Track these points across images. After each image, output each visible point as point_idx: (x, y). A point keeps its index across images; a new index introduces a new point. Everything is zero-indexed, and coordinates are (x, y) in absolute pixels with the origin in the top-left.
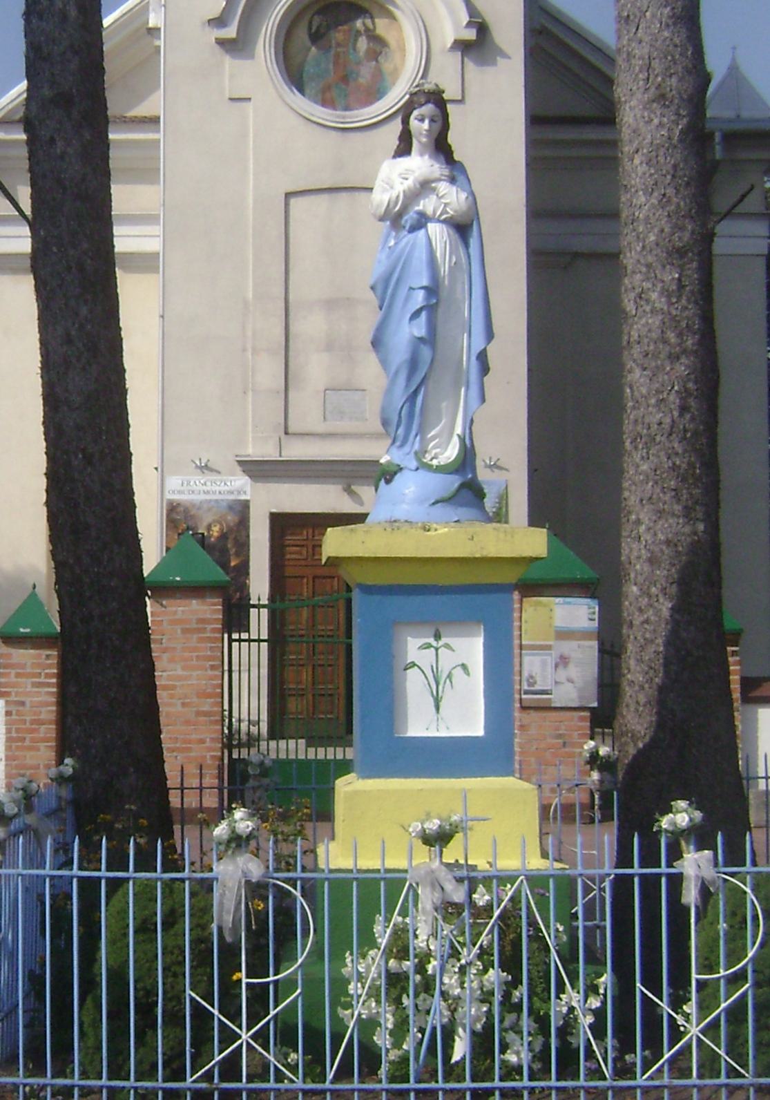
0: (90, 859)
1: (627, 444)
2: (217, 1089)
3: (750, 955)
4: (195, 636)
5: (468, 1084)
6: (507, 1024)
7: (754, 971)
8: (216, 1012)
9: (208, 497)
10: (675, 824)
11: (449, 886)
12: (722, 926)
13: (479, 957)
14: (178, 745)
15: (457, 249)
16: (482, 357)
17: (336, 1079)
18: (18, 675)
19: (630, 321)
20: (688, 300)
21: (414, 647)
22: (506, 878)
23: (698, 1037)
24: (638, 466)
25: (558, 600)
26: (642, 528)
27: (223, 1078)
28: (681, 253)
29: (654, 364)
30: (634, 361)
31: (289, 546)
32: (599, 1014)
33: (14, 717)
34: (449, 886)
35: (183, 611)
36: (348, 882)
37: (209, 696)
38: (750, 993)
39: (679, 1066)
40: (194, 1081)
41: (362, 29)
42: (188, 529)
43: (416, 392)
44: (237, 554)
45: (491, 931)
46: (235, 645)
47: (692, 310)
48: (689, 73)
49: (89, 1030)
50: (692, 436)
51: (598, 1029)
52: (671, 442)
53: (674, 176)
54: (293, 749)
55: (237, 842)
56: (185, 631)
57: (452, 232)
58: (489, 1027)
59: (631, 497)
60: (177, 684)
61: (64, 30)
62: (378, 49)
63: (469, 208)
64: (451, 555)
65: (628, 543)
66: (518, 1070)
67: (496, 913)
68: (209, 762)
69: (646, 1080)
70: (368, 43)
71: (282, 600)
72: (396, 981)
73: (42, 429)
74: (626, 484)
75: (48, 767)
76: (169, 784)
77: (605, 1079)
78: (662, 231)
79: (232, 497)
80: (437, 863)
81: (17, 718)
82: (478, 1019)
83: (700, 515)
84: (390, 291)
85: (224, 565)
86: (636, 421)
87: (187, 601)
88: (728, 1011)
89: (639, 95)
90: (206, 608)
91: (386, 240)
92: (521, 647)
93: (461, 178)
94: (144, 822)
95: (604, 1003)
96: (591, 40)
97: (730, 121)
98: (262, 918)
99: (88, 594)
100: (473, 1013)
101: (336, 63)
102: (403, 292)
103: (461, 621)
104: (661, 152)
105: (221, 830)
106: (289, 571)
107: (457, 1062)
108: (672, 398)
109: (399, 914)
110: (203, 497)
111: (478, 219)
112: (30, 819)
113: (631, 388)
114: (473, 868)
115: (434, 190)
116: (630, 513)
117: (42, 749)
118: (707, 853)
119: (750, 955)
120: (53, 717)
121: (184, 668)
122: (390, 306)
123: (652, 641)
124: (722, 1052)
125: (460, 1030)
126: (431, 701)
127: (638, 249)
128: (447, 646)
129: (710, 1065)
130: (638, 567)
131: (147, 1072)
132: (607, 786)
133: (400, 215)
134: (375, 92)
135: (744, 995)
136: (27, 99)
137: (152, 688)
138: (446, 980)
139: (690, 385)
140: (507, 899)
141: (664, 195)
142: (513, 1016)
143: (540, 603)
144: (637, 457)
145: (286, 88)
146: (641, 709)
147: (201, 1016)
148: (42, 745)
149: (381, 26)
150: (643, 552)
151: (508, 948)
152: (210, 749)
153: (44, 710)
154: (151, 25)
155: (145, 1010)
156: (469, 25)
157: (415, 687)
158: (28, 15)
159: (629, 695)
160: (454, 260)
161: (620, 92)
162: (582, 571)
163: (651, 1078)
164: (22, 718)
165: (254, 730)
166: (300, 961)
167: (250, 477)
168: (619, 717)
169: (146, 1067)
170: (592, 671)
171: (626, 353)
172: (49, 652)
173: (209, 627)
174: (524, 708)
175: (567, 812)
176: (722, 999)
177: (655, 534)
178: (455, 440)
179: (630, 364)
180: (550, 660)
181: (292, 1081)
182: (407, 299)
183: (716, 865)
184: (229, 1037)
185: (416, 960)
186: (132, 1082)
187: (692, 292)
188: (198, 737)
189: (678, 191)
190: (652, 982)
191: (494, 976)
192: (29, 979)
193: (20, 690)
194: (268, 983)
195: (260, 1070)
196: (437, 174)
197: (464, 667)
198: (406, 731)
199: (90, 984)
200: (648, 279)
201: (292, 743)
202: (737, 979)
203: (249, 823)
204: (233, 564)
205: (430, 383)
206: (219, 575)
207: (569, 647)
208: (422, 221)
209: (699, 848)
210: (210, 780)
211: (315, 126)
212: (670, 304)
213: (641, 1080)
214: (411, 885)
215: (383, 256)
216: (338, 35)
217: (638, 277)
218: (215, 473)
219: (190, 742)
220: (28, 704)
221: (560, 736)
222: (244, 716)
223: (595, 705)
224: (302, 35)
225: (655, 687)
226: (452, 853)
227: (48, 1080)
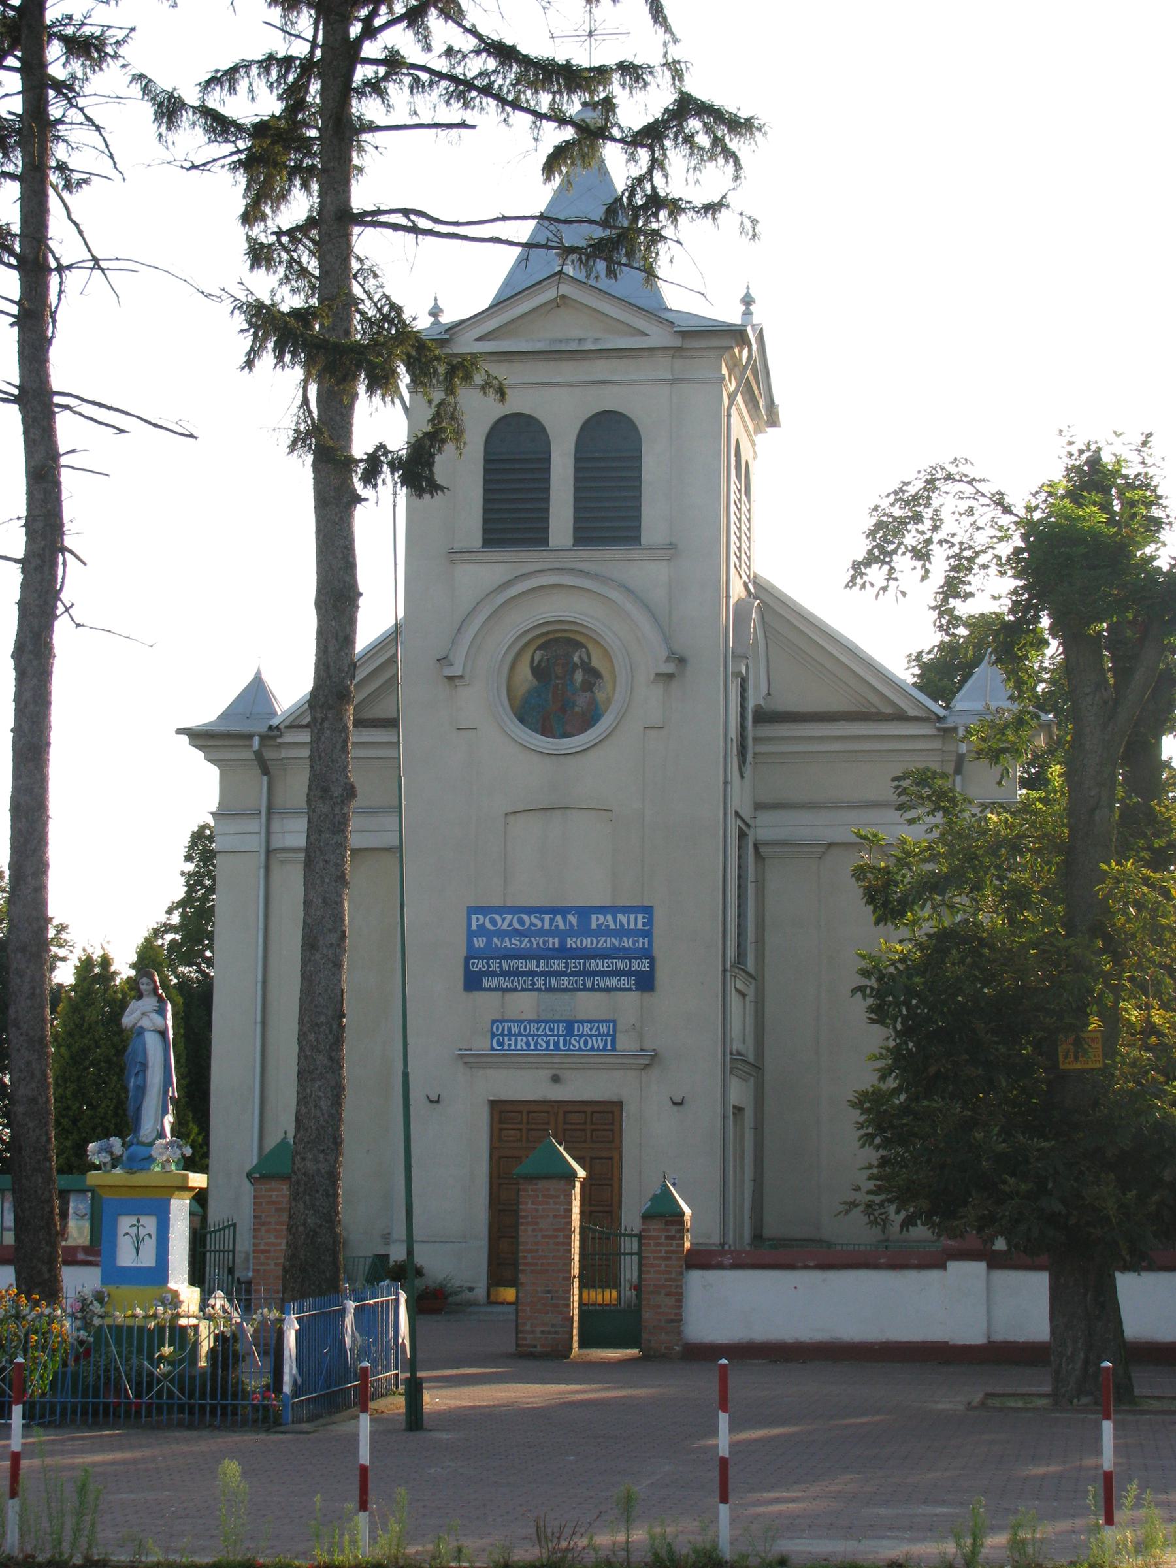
56: (277, 1210)
62: (592, 680)
70: (584, 675)
96: (843, 641)
126: (135, 1251)
213: (146, 1400)
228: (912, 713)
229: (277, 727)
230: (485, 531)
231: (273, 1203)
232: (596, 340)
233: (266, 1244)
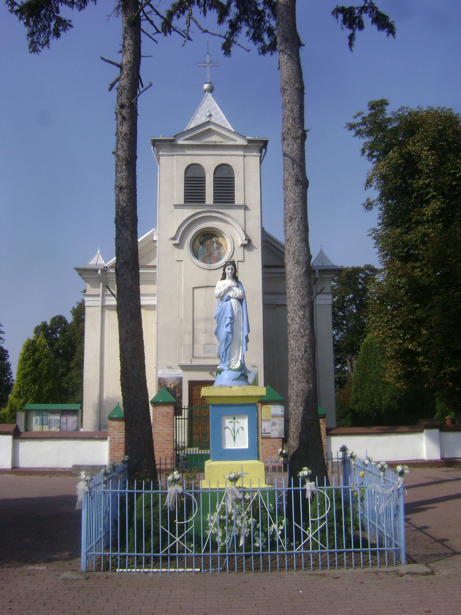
0: (131, 487)
1: (290, 362)
2: (169, 555)
3: (326, 513)
5: (244, 553)
6: (255, 534)
7: (327, 518)
8: (169, 532)
10: (304, 474)
11: (237, 494)
12: (318, 504)
13: (247, 514)
15: (239, 306)
16: (247, 337)
17: (205, 551)
18: (113, 429)
19: (290, 326)
20: (307, 320)
21: (228, 422)
22: (254, 491)
23: (312, 538)
24: (293, 368)
25: (272, 406)
26: (294, 386)
27: (171, 552)
28: (304, 306)
29: (297, 338)
30: (291, 337)
32: (283, 531)
34: (237, 494)
36: (208, 493)
37: (170, 435)
38: (327, 524)
39: (306, 546)
40: (162, 553)
42: (164, 386)
43: (227, 348)
44: (179, 393)
45: (250, 507)
46: (178, 420)
47: (308, 323)
48: (306, 255)
49: (131, 538)
50: (308, 359)
51: (282, 536)
52: (302, 361)
53: (302, 285)
54: (195, 451)
55: (175, 481)
56: (163, 416)
57: (238, 301)
58: (250, 536)
59: (291, 377)
60: (160, 432)
61: (127, 243)
62: (219, 247)
63: (242, 295)
64: (237, 395)
65: (290, 391)
66: (259, 548)
67: (251, 502)
68: (170, 455)
69: (297, 550)
71: (192, 407)
72: (222, 522)
73: (119, 358)
74: (289, 373)
75: (122, 456)
76: (156, 463)
77: (284, 551)
78: (299, 300)
79: (177, 376)
80: (234, 487)
82: (247, 533)
83: (311, 382)
84: (220, 319)
85: (174, 396)
86: (292, 355)
88: (320, 529)
89: (291, 262)
91: (219, 304)
92: (262, 420)
93: (240, 286)
94: (149, 474)
95: (284, 528)
97: (321, 266)
98: (182, 503)
99: (132, 406)
100: (245, 531)
102: (224, 319)
103: (241, 414)
104: (298, 277)
105: (170, 478)
106: (194, 398)
107: (241, 546)
108: (302, 348)
109: (223, 501)
110: (168, 376)
111: (245, 298)
112: (115, 474)
113: (290, 345)
114: (245, 488)
115: (232, 289)
116: (290, 382)
117: (121, 451)
118: (313, 483)
119: (326, 513)
120: (123, 442)
121: (162, 427)
122: (220, 323)
123: (298, 419)
124: (319, 542)
125: (242, 536)
127: (292, 305)
128: (237, 422)
129: (315, 546)
130: (293, 397)
131: (148, 550)
132: (285, 462)
133: (223, 297)
135: (325, 525)
136: (116, 263)
137: (151, 434)
138: (237, 522)
139: (307, 345)
140: (255, 497)
141: (299, 290)
142: (257, 532)
143: (267, 407)
144: (292, 365)
145: (193, 257)
146: (295, 439)
147: (164, 534)
148: (120, 450)
150: (295, 393)
151: (256, 511)
152: (171, 451)
153: (121, 440)
154: (154, 240)
155: (148, 531)
156: (245, 240)
157: (228, 434)
158: (116, 239)
159: (291, 434)
160: (238, 309)
161: (286, 261)
162: (279, 397)
163: (298, 550)
165: (183, 445)
166: (193, 516)
167: (183, 370)
168: (288, 442)
169: (148, 548)
170: (283, 427)
171: (289, 335)
173: (170, 415)
174: (262, 438)
175: (274, 469)
176: (319, 526)
177: (298, 388)
178: (239, 361)
179: (290, 339)
180: (270, 424)
181: (192, 553)
182: (225, 321)
183: (316, 486)
184: (172, 540)
185: (228, 516)
186: (144, 554)
187: (308, 318)
189: (303, 289)
190: (298, 521)
191: (251, 520)
192: (114, 522)
194: (184, 524)
195: (182, 549)
196: (233, 285)
197: (242, 428)
198: (225, 447)
199: (131, 524)
200: (295, 314)
201: (194, 449)
202: (323, 520)
203: (178, 475)
204: (177, 396)
205: (232, 345)
206: (173, 399)
207: (276, 420)
208: (229, 298)
209: (311, 481)
210: (169, 461)
212: (301, 321)
213: (295, 551)
214: (226, 493)
215: (218, 308)
216: (208, 242)
217: (292, 313)
220: (116, 438)
221: (273, 446)
222: (180, 440)
223: (284, 437)
224: (198, 243)
225: (299, 432)
226: (238, 484)
227: (119, 553)
229: (107, 267)
232: (220, 142)
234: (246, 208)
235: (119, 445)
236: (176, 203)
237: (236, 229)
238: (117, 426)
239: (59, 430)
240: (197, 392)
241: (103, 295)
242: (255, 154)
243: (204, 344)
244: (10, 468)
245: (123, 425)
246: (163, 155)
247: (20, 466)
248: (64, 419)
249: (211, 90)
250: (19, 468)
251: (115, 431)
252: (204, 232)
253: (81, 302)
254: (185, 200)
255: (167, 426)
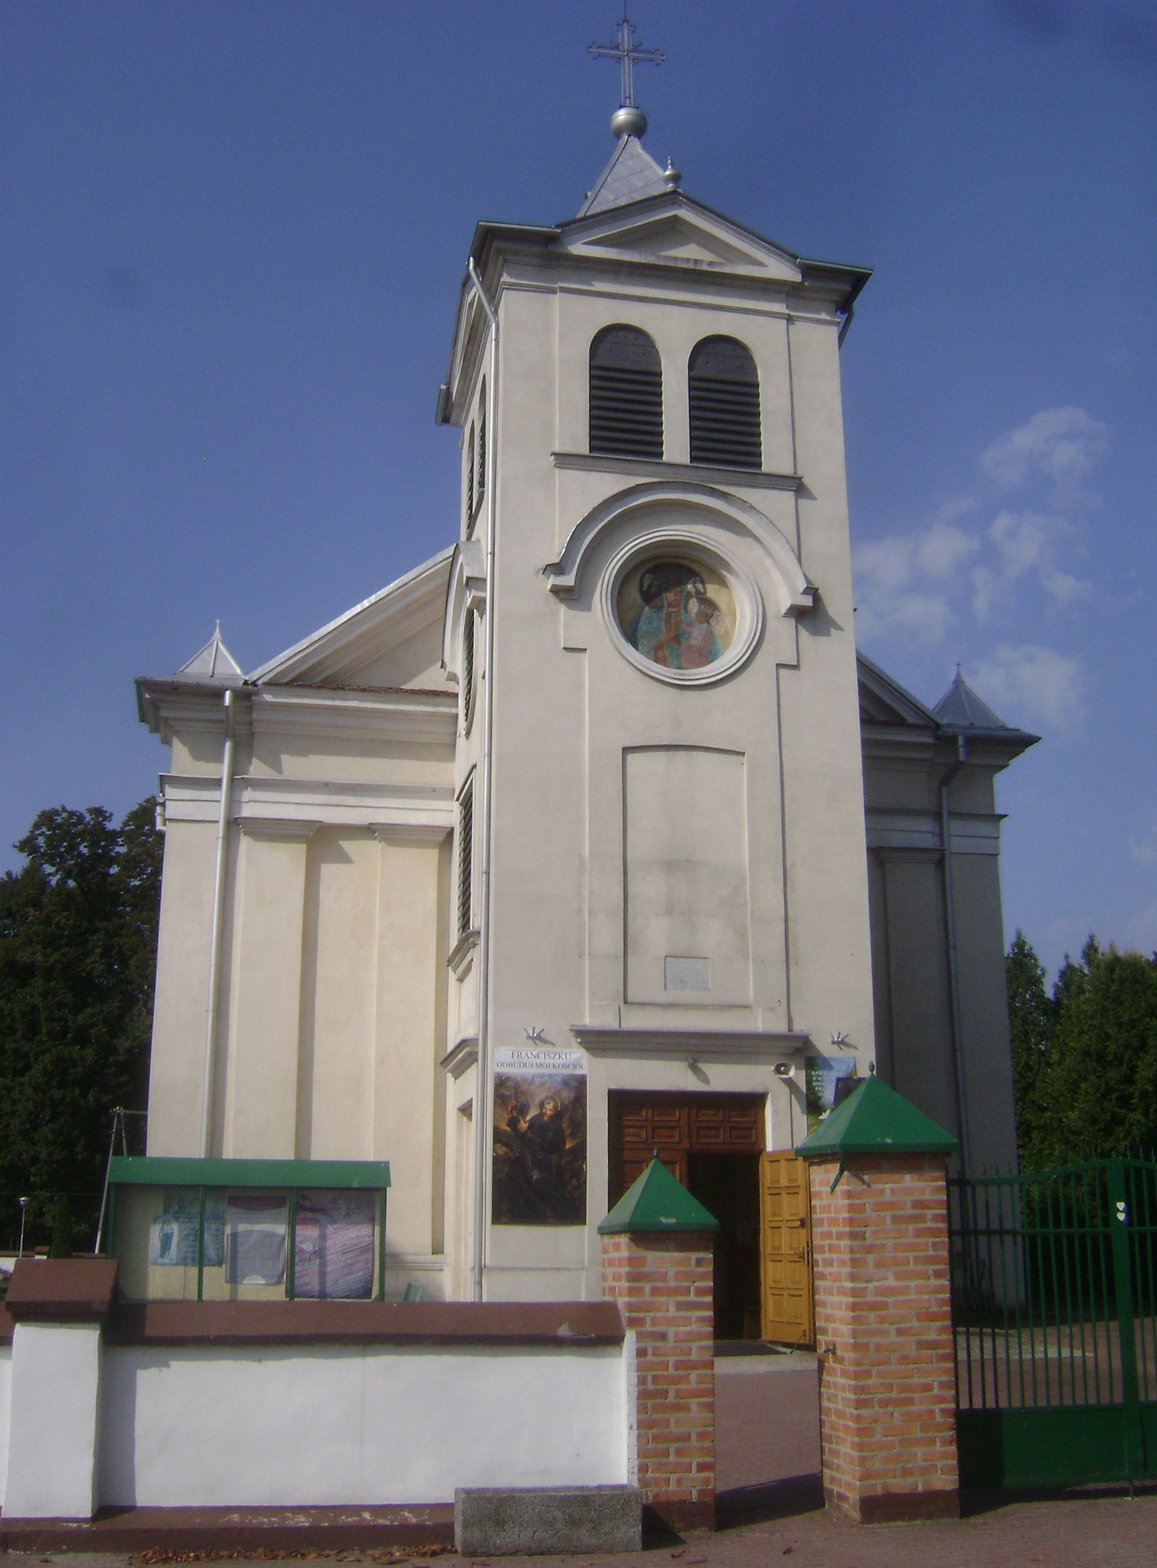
4: (911, 1227)
9: (541, 1071)
14: (894, 1394)
18: (655, 1291)
31: (627, 1127)
33: (650, 1358)
35: (892, 1190)
41: (693, 591)
44: (573, 1135)
56: (896, 1219)
60: (890, 1300)
62: (709, 612)
68: (939, 1418)
79: (567, 1072)
81: (655, 1359)
87: (897, 1176)
90: (923, 1184)
101: (668, 621)
121: (897, 1277)
134: (707, 655)
149: (712, 591)
152: (940, 1399)
153: (694, 1345)
156: (806, 591)
164: (662, 1359)
167: (587, 1049)
172: (701, 1255)
173: (930, 1213)
188: (923, 1380)
193: (659, 1315)
204: (568, 1146)
211: (653, 682)
218: (548, 1045)
219: (911, 1388)
220: (671, 1337)
228: (911, 719)
229: (254, 684)
230: (592, 438)
231: (891, 1205)
233: (879, 1291)
234: (796, 485)
235: (681, 1372)
236: (558, 449)
237: (770, 555)
238: (671, 1273)
239: (278, 1294)
240: (639, 1135)
241: (232, 781)
242: (824, 316)
243: (663, 955)
244: (87, 1513)
245: (701, 1269)
246: (521, 285)
247: (138, 1505)
248: (308, 1236)
249: (638, 129)
250: (132, 1509)
251: (663, 1299)
252: (656, 558)
253: (6, 879)
254: (593, 443)
255: (919, 1267)
